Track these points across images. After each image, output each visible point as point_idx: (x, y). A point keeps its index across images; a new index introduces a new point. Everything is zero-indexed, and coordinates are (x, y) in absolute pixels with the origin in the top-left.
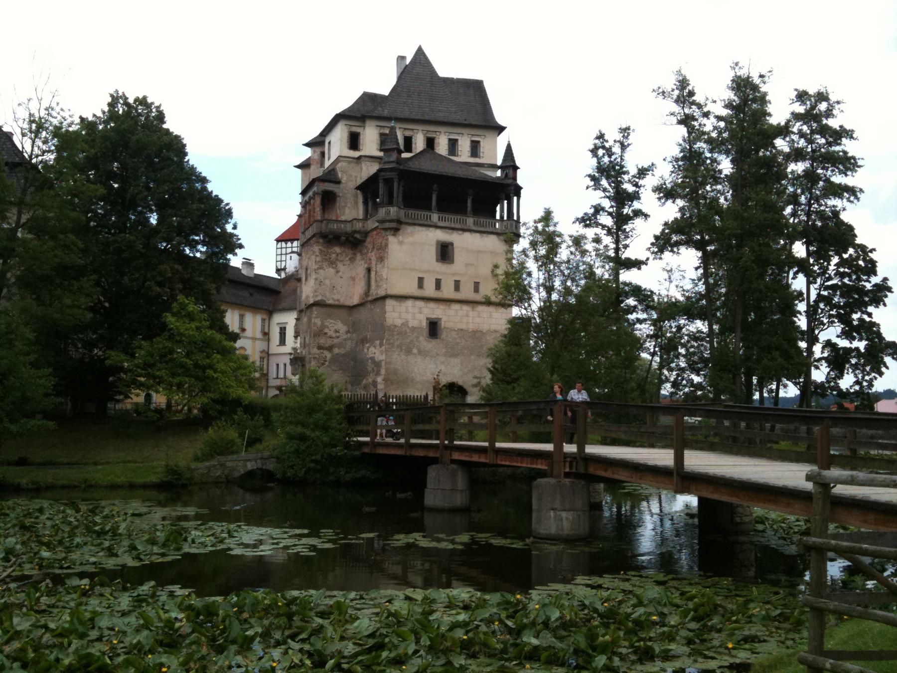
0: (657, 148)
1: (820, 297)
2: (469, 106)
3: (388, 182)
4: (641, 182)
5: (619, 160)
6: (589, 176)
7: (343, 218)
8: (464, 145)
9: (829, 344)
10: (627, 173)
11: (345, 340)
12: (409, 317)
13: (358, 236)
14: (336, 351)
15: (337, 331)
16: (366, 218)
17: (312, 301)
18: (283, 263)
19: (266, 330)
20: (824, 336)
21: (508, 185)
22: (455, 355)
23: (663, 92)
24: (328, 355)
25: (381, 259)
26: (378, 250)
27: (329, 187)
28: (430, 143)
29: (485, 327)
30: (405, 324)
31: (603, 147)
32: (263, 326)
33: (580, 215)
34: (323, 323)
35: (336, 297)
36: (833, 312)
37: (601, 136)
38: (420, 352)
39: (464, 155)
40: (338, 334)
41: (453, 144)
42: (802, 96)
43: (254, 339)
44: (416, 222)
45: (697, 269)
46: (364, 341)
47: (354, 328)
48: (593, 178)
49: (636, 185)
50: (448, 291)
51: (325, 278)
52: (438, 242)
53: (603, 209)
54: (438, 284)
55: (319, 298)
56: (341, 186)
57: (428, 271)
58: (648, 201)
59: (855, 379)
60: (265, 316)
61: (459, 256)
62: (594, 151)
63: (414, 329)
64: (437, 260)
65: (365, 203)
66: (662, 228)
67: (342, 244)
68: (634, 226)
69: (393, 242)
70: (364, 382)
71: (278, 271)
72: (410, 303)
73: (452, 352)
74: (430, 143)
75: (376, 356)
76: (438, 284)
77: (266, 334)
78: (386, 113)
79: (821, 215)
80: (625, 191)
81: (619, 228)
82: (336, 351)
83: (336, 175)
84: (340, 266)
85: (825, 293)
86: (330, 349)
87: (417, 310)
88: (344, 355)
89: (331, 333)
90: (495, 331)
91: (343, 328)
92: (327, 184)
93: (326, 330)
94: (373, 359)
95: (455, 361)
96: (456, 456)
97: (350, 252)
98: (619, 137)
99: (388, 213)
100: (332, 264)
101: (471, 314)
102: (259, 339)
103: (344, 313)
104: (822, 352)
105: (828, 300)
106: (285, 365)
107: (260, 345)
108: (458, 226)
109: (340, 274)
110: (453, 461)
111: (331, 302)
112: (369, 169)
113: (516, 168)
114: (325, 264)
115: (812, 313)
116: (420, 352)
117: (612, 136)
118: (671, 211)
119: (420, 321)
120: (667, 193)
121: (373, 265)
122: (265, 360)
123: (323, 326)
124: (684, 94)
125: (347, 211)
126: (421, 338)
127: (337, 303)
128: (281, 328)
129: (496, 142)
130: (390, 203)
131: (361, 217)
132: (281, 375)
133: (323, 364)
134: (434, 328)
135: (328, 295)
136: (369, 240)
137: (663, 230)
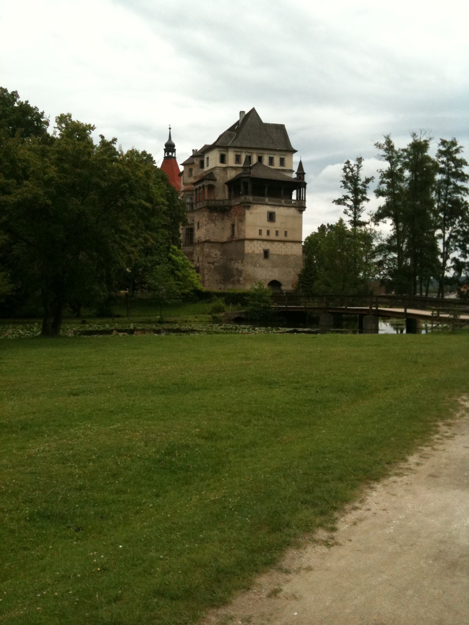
0: (374, 167)
1: (451, 236)
2: (277, 138)
3: (246, 184)
4: (367, 185)
5: (356, 174)
6: (342, 181)
7: (218, 198)
8: (277, 160)
9: (454, 260)
10: (360, 180)
11: (220, 259)
12: (255, 249)
13: (227, 208)
14: (216, 264)
15: (216, 255)
17: (203, 240)
20: (452, 256)
21: (300, 183)
22: (275, 267)
23: (380, 146)
24: (212, 267)
27: (211, 182)
28: (260, 159)
29: (289, 253)
30: (253, 252)
31: (349, 167)
33: (337, 199)
35: (215, 238)
36: (457, 244)
37: (348, 162)
38: (260, 266)
39: (277, 165)
41: (271, 160)
42: (443, 143)
45: (391, 225)
46: (231, 260)
47: (224, 253)
48: (344, 182)
49: (365, 186)
50: (273, 236)
53: (349, 198)
54: (268, 232)
55: (207, 239)
56: (217, 182)
57: (264, 226)
58: (371, 195)
61: (277, 219)
62: (345, 169)
63: (257, 255)
64: (268, 221)
66: (378, 209)
68: (363, 205)
69: (248, 213)
70: (232, 279)
72: (255, 242)
73: (274, 266)
74: (260, 159)
76: (268, 232)
79: (450, 201)
80: (359, 188)
81: (356, 208)
82: (216, 264)
83: (214, 176)
84: (217, 222)
85: (454, 234)
86: (213, 263)
87: (259, 245)
89: (213, 256)
90: (294, 255)
92: (210, 181)
93: (211, 254)
94: (237, 269)
95: (276, 270)
96: (330, 311)
98: (356, 163)
99: (246, 199)
100: (213, 221)
101: (283, 247)
104: (451, 263)
105: (455, 237)
108: (277, 204)
109: (217, 226)
110: (329, 312)
111: (213, 240)
112: (232, 175)
113: (304, 174)
114: (210, 222)
115: (446, 244)
116: (260, 266)
117: (353, 163)
118: (382, 201)
119: (260, 251)
120: (379, 193)
124: (390, 147)
126: (261, 259)
129: (292, 156)
130: (246, 193)
131: (227, 198)
134: (266, 254)
136: (232, 210)
137: (379, 210)
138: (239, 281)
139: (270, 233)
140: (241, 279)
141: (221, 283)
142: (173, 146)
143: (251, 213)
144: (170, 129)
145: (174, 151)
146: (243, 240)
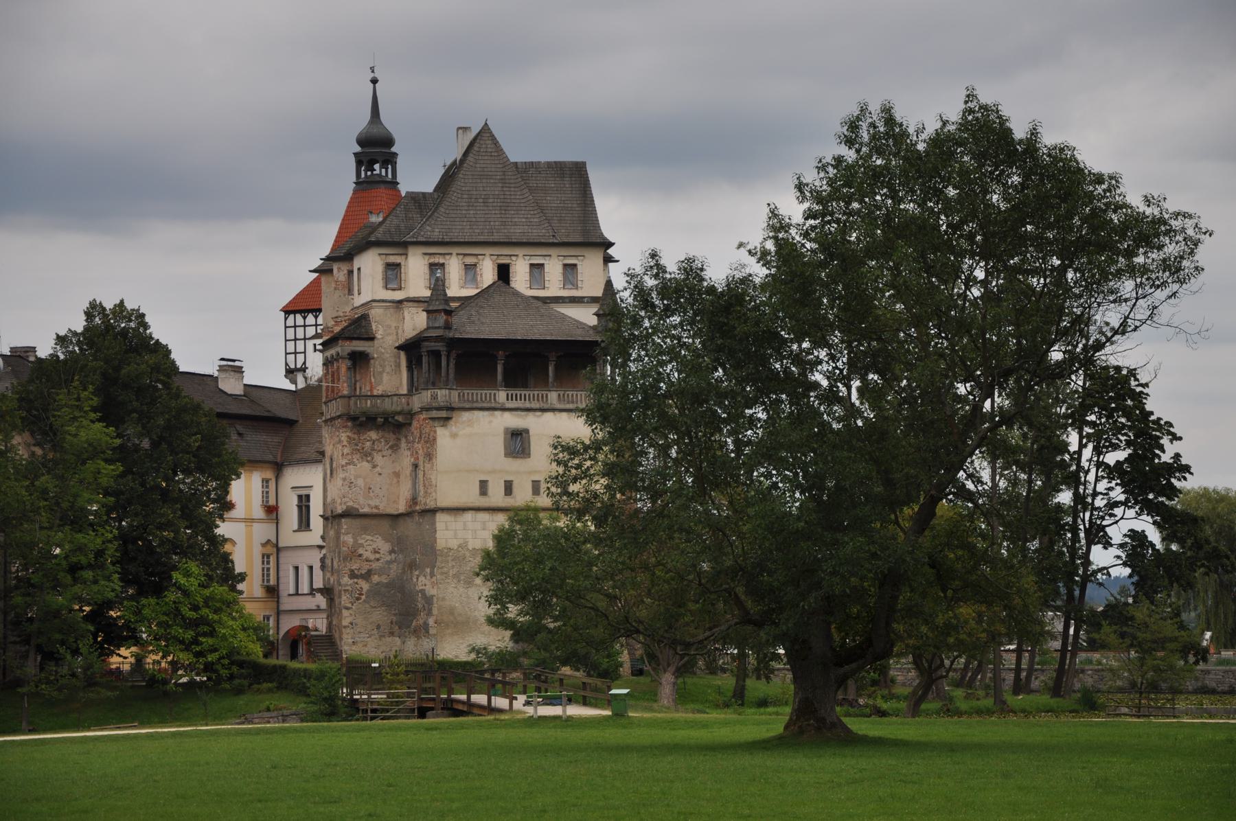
8: (554, 269)
11: (390, 562)
12: (469, 535)
13: (400, 418)
15: (376, 552)
16: (410, 393)
17: (339, 511)
18: (300, 358)
19: (272, 502)
24: (365, 586)
25: (430, 456)
26: (426, 442)
27: (359, 346)
28: (504, 273)
30: (463, 546)
32: (266, 495)
34: (356, 541)
35: (373, 503)
40: (377, 556)
43: (249, 521)
44: (475, 405)
46: (412, 566)
47: (399, 545)
51: (357, 477)
52: (507, 430)
54: (509, 488)
59: (487, 684)
60: (269, 474)
65: (410, 368)
67: (378, 428)
69: (443, 435)
71: (290, 373)
72: (469, 516)
74: (504, 273)
75: (427, 588)
76: (509, 488)
77: (272, 511)
78: (436, 235)
82: (375, 579)
84: (378, 458)
86: (367, 576)
88: (387, 585)
91: (384, 547)
92: (355, 343)
93: (361, 551)
94: (423, 591)
97: (392, 436)
99: (434, 397)
100: (367, 455)
102: (259, 521)
103: (386, 524)
106: (311, 568)
107: (263, 531)
108: (535, 405)
109: (378, 469)
111: (366, 510)
112: (415, 322)
114: (356, 457)
121: (421, 463)
122: (272, 485)
123: (357, 545)
125: (385, 377)
127: (375, 511)
128: (300, 497)
131: (405, 392)
132: (305, 588)
133: (358, 599)
135: (362, 500)
136: (415, 423)
138: (426, 627)
139: (490, 490)
140: (431, 621)
141: (392, 634)
142: (388, 141)
143: (454, 436)
144: (374, 81)
145: (390, 160)
146: (434, 511)
